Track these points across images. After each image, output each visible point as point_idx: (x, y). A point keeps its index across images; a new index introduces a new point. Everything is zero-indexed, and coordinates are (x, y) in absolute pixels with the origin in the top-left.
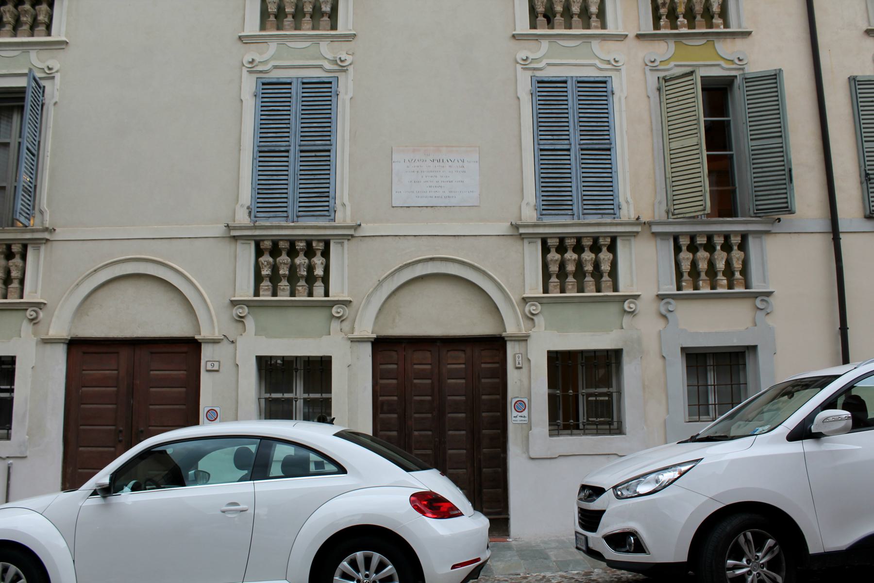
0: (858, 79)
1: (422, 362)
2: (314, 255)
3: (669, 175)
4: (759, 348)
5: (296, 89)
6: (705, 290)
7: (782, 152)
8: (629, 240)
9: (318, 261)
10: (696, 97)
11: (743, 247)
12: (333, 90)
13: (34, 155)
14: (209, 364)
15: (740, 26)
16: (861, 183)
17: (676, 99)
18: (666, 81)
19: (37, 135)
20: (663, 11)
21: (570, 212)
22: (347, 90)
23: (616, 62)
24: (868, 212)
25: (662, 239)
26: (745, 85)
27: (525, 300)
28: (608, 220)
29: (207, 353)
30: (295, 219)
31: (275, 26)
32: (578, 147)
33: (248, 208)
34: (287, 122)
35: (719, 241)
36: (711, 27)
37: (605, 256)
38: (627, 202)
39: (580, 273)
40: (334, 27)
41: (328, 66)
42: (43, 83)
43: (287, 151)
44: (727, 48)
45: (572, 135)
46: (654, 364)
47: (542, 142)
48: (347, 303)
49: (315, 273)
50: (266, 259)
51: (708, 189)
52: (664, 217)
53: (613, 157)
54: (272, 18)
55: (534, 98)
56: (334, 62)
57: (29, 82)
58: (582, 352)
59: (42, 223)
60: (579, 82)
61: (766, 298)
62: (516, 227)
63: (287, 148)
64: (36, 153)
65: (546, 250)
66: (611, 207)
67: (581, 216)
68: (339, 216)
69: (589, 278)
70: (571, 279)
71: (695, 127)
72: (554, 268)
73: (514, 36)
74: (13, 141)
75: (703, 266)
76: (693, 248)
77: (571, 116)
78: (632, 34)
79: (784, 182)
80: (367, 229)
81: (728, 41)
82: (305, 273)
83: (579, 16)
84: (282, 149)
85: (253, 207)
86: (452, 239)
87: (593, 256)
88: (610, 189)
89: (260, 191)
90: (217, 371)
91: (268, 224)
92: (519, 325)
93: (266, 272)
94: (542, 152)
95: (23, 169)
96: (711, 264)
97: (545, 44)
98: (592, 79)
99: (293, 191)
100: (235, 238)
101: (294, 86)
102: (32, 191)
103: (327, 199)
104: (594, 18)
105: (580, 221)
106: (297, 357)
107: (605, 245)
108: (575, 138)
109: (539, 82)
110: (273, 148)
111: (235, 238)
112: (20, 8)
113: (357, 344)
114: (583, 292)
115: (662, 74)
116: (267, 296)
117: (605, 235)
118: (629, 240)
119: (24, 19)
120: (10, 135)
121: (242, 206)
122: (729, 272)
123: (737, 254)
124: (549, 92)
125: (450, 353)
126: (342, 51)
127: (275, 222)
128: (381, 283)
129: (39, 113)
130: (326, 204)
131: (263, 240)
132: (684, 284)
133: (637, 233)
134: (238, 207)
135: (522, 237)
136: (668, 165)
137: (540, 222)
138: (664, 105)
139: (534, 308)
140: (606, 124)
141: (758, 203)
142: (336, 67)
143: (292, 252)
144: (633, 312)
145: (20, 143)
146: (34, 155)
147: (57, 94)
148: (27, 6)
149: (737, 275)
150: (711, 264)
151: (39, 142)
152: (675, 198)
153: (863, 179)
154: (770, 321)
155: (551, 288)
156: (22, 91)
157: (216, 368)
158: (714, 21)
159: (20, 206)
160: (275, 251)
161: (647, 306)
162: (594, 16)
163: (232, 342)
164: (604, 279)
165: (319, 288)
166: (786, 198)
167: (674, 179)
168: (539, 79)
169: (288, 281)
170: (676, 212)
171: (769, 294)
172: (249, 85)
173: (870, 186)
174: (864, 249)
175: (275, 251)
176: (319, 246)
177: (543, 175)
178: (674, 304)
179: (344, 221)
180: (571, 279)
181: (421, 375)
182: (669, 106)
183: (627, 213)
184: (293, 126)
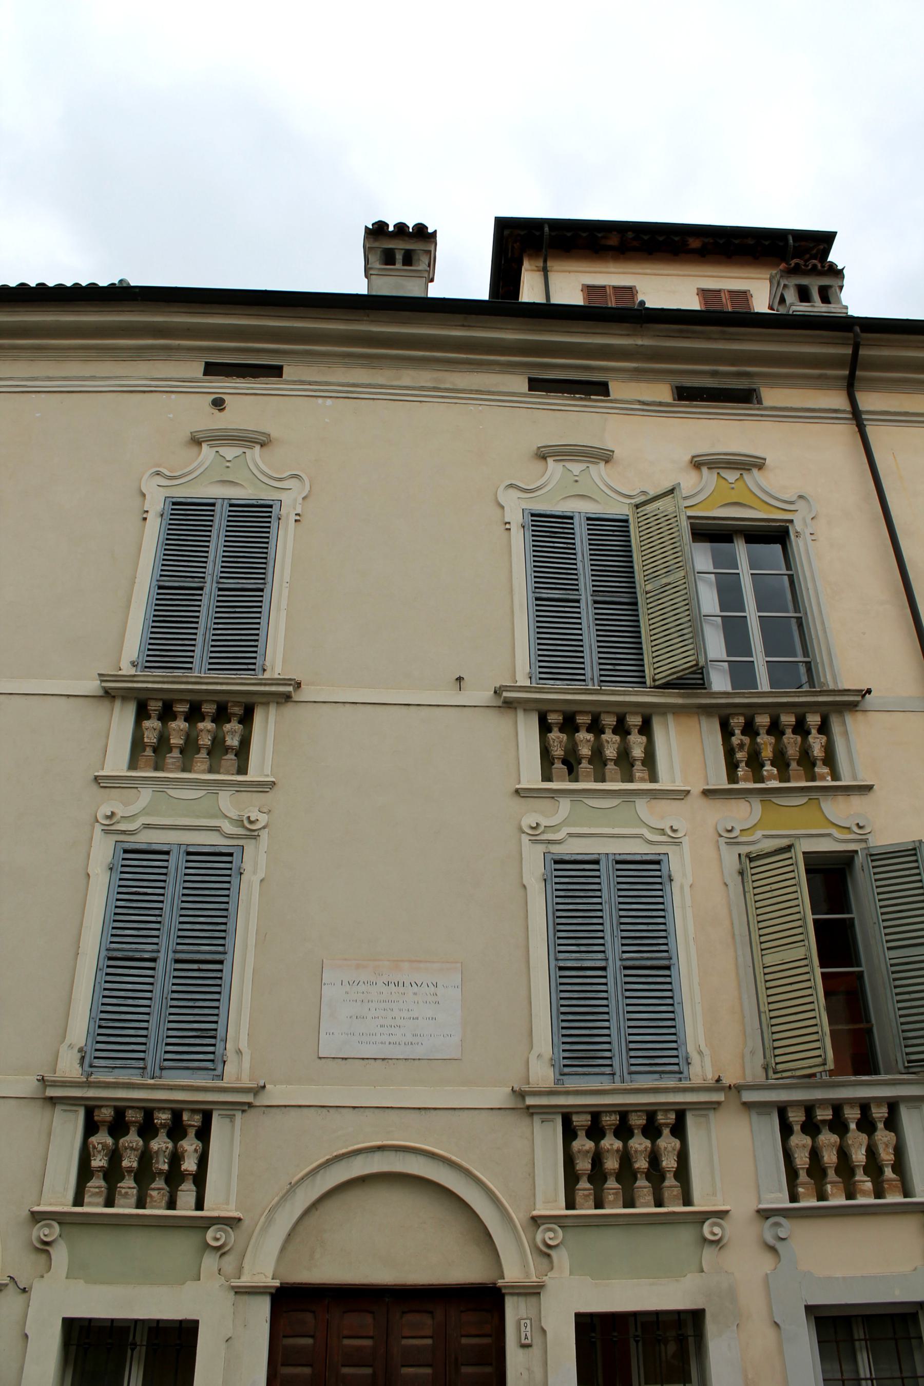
1: (357, 1333)
5: (176, 862)
6: (838, 1200)
8: (706, 1116)
9: (190, 1145)
11: (892, 1123)
12: (234, 866)
15: (855, 778)
21: (607, 1070)
22: (255, 865)
23: (675, 831)
25: (759, 1114)
26: (871, 864)
27: (536, 1221)
28: (670, 1082)
32: (619, 963)
34: (157, 912)
35: (852, 1115)
36: (813, 779)
37: (668, 1143)
38: (700, 1053)
39: (626, 1173)
40: (242, 770)
43: (154, 960)
44: (838, 810)
45: (609, 945)
46: (760, 1337)
48: (232, 1222)
49: (183, 1167)
50: (102, 1139)
51: (827, 1029)
52: (760, 1078)
53: (674, 980)
54: (149, 752)
55: (549, 887)
56: (239, 823)
58: (635, 1315)
60: (618, 862)
62: (521, 1095)
63: (154, 955)
65: (569, 1133)
68: (230, 1070)
69: (642, 1182)
72: (584, 1165)
73: (517, 791)
75: (830, 1157)
76: (811, 1128)
78: (696, 789)
80: (276, 1094)
81: (840, 799)
82: (166, 1167)
83: (616, 762)
84: (146, 955)
87: (648, 1143)
88: (672, 1031)
89: (104, 1023)
91: (111, 1079)
92: (525, 1265)
93: (99, 1162)
94: (563, 973)
96: (843, 1154)
97: (565, 804)
98: (638, 858)
100: (53, 1101)
101: (173, 858)
103: (212, 1041)
104: (638, 765)
106: (136, 1321)
107: (666, 1125)
108: (614, 949)
109: (556, 862)
110: (131, 954)
111: (53, 1101)
113: (245, 1298)
114: (632, 1205)
115: (744, 850)
116: (97, 1205)
117: (666, 1107)
121: (70, 1046)
123: (884, 1137)
124: (572, 879)
126: (252, 807)
128: (293, 1187)
130: (211, 1049)
131: (100, 1107)
132: (800, 1190)
134: (63, 1048)
135: (531, 1111)
137: (560, 1088)
139: (551, 1235)
140: (662, 927)
143: (148, 1130)
144: (717, 1242)
149: (888, 1173)
150: (843, 1154)
152: (776, 1044)
155: (579, 1200)
158: (816, 770)
160: (118, 1127)
161: (741, 1230)
162: (638, 763)
163: (24, 1290)
167: (773, 1014)
168: (557, 858)
169: (136, 1181)
170: (780, 1067)
172: (103, 851)
175: (118, 1127)
176: (192, 1120)
177: (563, 1009)
178: (787, 1227)
179: (238, 1079)
181: (355, 1358)
182: (758, 898)
183: (701, 1070)
184: (166, 919)
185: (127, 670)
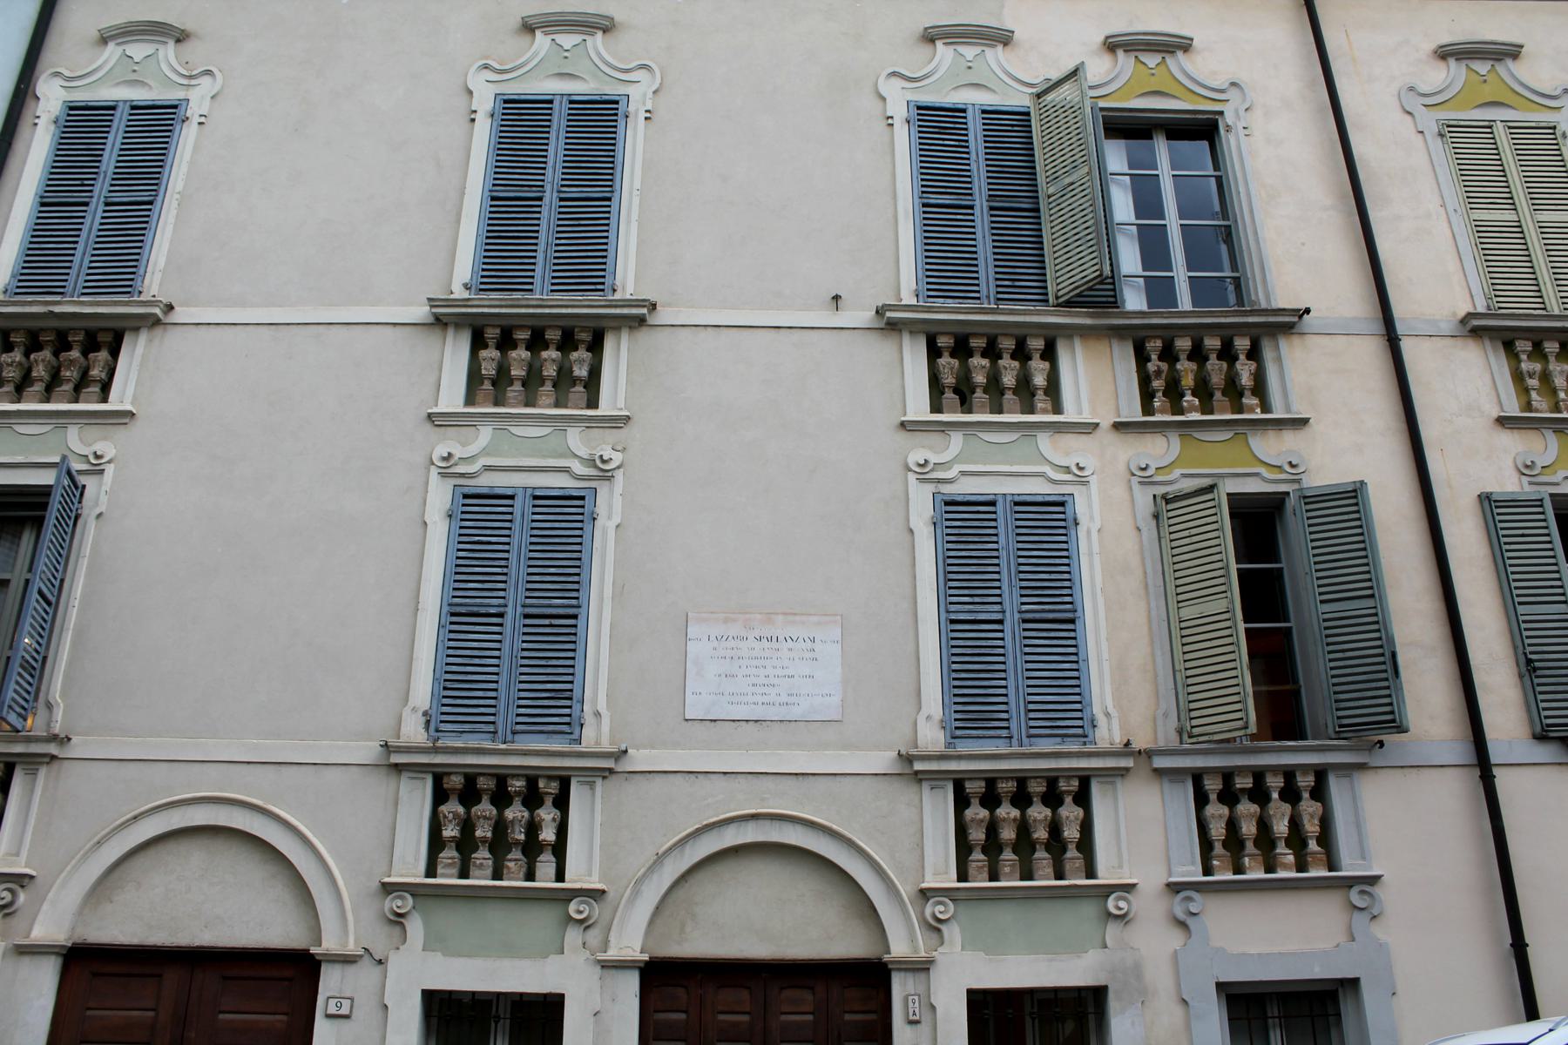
0: (1495, 497)
2: (540, 804)
3: (1180, 666)
4: (1363, 983)
7: (1377, 623)
8: (1113, 783)
9: (547, 814)
10: (1221, 529)
13: (49, 603)
14: (332, 1002)
16: (1521, 676)
17: (1186, 533)
18: (1168, 502)
19: (60, 568)
20: (1157, 384)
21: (1004, 733)
22: (610, 510)
23: (1081, 469)
24: (1538, 729)
25: (1171, 781)
27: (925, 894)
29: (330, 982)
30: (510, 736)
31: (491, 398)
32: (1017, 616)
33: (425, 714)
34: (503, 563)
35: (1275, 783)
36: (1241, 412)
37: (1070, 812)
38: (1107, 715)
39: (1024, 844)
40: (593, 403)
41: (578, 468)
42: (82, 480)
43: (501, 615)
44: (1268, 446)
45: (1006, 595)
46: (1167, 1014)
47: (953, 608)
48: (596, 895)
50: (453, 808)
51: (1250, 689)
52: (1174, 741)
53: (1079, 634)
54: (487, 385)
56: (591, 462)
57: (58, 479)
58: (1031, 992)
59: (48, 725)
60: (1016, 504)
61: (1367, 888)
62: (907, 759)
64: (53, 600)
65: (961, 802)
66: (1079, 723)
67: (1025, 740)
68: (588, 734)
69: (1041, 854)
70: (1008, 855)
71: (1221, 580)
72: (977, 835)
73: (903, 425)
74: (17, 578)
75: (1249, 829)
76: (1229, 797)
77: (1003, 562)
78: (1106, 421)
79: (1383, 675)
80: (640, 759)
82: (522, 837)
83: (1015, 391)
84: (493, 611)
85: (433, 713)
86: (791, 781)
87: (1048, 812)
88: (1077, 690)
89: (449, 685)
90: (347, 1017)
91: (459, 744)
92: (913, 939)
93: (450, 832)
94: (953, 625)
95: (27, 628)
96: (1264, 825)
97: (957, 440)
98: (1040, 499)
99: (507, 685)
100: (398, 768)
101: (518, 503)
102: (37, 668)
103: (567, 703)
104: (1040, 395)
105: (1023, 750)
106: (499, 994)
107: (1069, 792)
108: (1012, 601)
109: (947, 503)
110: (475, 609)
111: (398, 768)
112: (63, 355)
113: (613, 972)
114: (1031, 878)
116: (451, 876)
117: (1069, 773)
118: (1113, 783)
119: (66, 373)
120: (14, 565)
121: (414, 709)
122: (1297, 839)
123: (1309, 807)
124: (964, 520)
125: (788, 993)
126: (604, 445)
127: (473, 742)
128: (660, 858)
129: (69, 531)
131: (450, 774)
133: (1127, 769)
134: (406, 712)
135: (919, 777)
136: (1178, 649)
137: (951, 751)
138: (1166, 543)
139: (942, 908)
140: (1066, 576)
141: (1341, 713)
142: (593, 472)
143: (501, 798)
145: (27, 581)
146: (49, 603)
147: (104, 499)
148: (75, 354)
149: (1313, 845)
150: (1264, 825)
151: (62, 581)
152: (1193, 706)
153: (1524, 669)
154: (1379, 931)
155: (972, 871)
156: (44, 492)
157: (345, 1011)
158: (1244, 400)
159: (11, 694)
160: (469, 795)
161: (1149, 905)
162: (1040, 392)
163: (380, 962)
164: (1069, 855)
165: (546, 865)
166: (1391, 704)
167: (1190, 673)
168: (948, 498)
170: (1196, 731)
171: (1373, 880)
173: (1536, 681)
174: (1538, 793)
175: (469, 795)
176: (549, 788)
177: (955, 667)
178: (1198, 902)
179: (598, 743)
180: (1008, 855)
183: (1108, 734)
185: (459, 293)
